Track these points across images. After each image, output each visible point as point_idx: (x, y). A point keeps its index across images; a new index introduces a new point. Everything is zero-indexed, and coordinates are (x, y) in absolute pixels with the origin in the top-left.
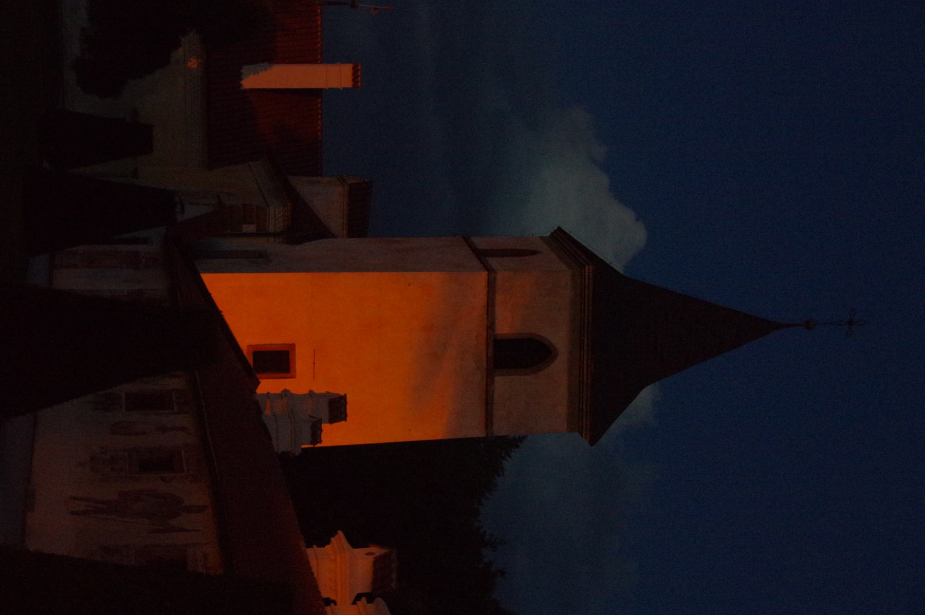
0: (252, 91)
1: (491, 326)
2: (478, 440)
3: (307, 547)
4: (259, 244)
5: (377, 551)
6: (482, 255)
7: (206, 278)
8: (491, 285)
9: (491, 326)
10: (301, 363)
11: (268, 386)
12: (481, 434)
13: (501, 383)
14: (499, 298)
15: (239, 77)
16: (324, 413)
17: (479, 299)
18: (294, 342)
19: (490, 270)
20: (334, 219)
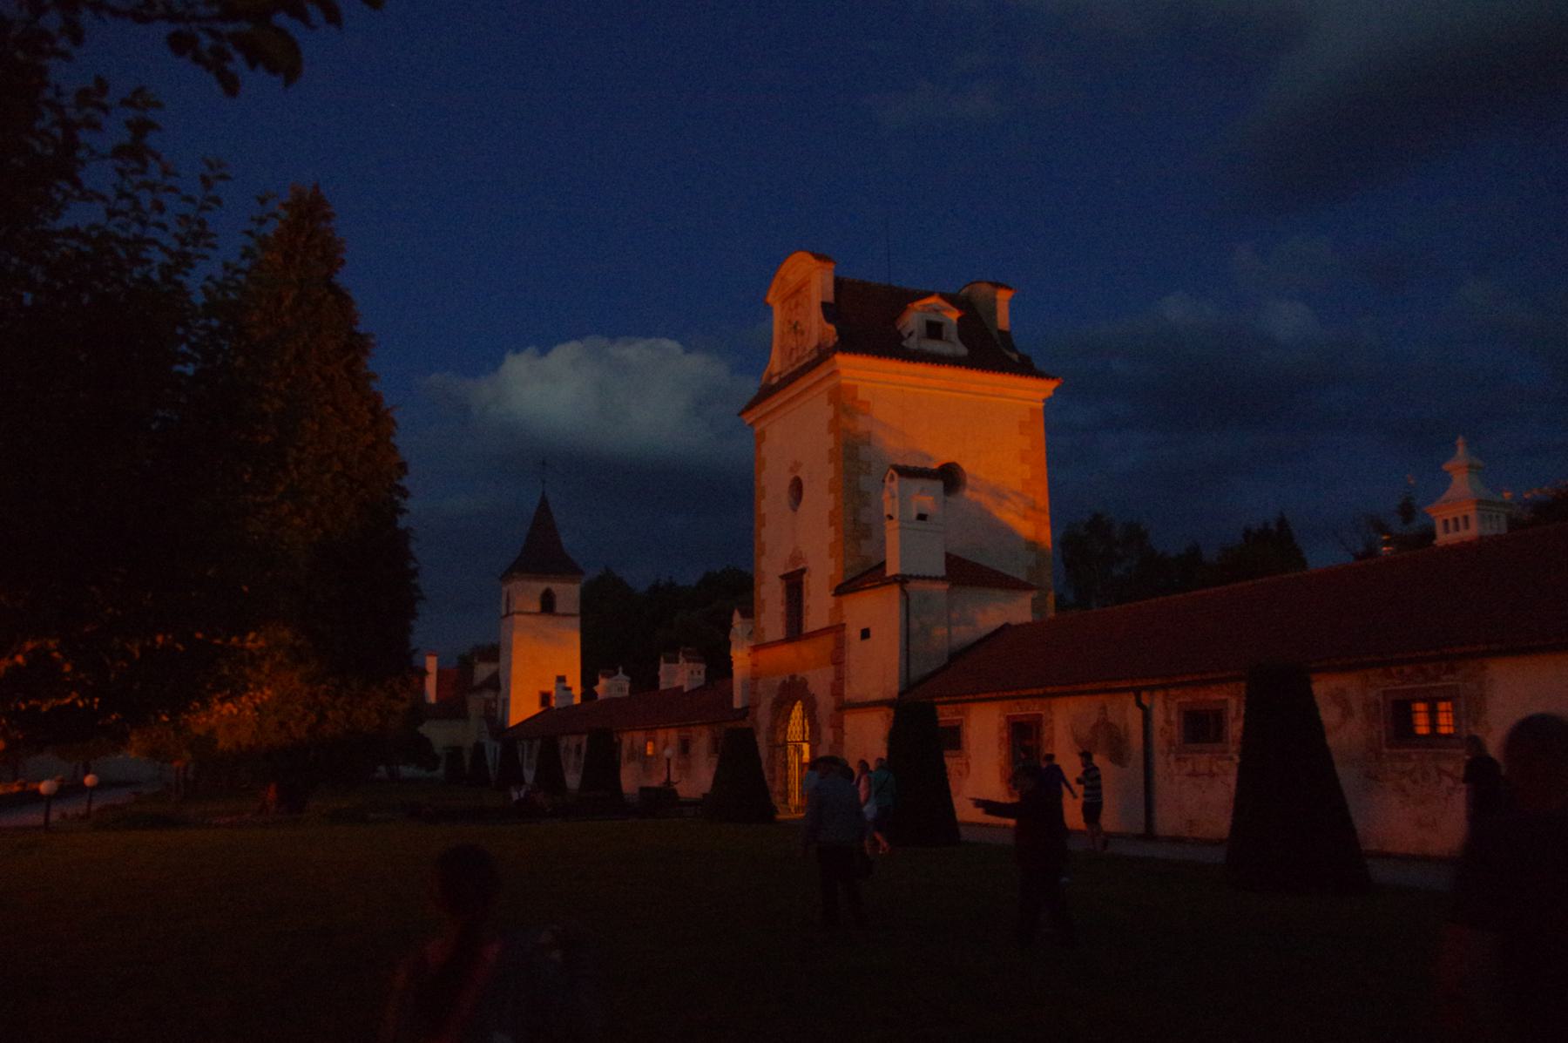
0: (437, 698)
1: (536, 614)
2: (582, 620)
3: (596, 698)
4: (500, 702)
5: (600, 677)
6: (508, 614)
7: (512, 723)
8: (520, 613)
9: (536, 614)
10: (547, 689)
11: (554, 703)
12: (578, 619)
13: (559, 609)
14: (525, 610)
15: (431, 705)
16: (562, 684)
17: (522, 617)
18: (555, 677)
19: (513, 613)
20: (493, 667)
